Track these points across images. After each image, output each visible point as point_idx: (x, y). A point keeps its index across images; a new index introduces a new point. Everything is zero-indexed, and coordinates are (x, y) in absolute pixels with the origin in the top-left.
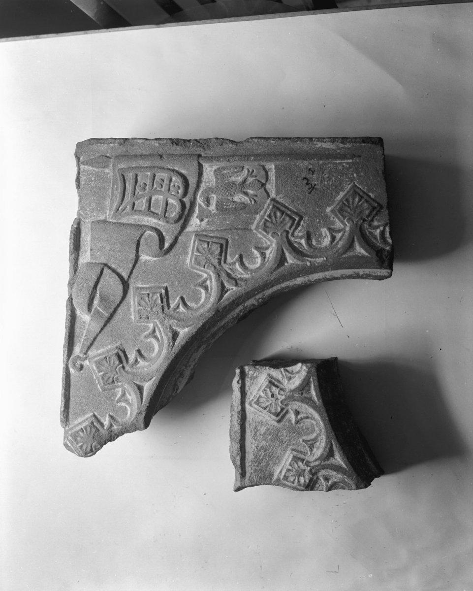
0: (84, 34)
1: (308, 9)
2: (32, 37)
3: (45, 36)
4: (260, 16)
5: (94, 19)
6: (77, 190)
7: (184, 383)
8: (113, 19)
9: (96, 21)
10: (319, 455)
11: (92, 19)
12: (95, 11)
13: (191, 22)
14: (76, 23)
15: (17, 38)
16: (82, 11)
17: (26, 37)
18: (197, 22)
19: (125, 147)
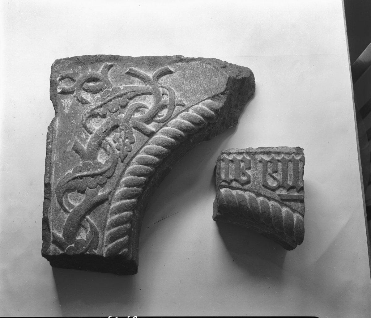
0: (348, 49)
1: (366, 205)
2: (348, 47)
3: (346, 23)
4: (361, 166)
5: (357, 60)
6: (255, 80)
7: (194, 63)
8: (359, 72)
9: (356, 61)
10: (224, 189)
11: (357, 58)
12: (363, 61)
13: (356, 120)
14: (355, 48)
15: (344, 4)
16: (363, 51)
17: (344, 10)
18: (356, 124)
19: (299, 173)
